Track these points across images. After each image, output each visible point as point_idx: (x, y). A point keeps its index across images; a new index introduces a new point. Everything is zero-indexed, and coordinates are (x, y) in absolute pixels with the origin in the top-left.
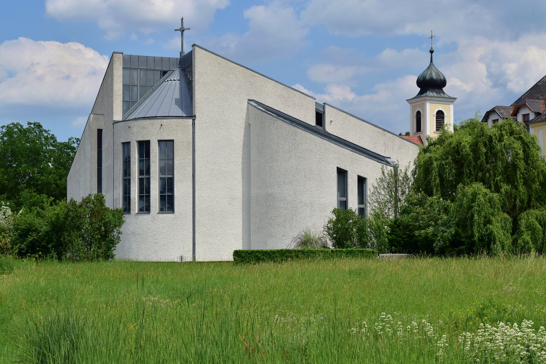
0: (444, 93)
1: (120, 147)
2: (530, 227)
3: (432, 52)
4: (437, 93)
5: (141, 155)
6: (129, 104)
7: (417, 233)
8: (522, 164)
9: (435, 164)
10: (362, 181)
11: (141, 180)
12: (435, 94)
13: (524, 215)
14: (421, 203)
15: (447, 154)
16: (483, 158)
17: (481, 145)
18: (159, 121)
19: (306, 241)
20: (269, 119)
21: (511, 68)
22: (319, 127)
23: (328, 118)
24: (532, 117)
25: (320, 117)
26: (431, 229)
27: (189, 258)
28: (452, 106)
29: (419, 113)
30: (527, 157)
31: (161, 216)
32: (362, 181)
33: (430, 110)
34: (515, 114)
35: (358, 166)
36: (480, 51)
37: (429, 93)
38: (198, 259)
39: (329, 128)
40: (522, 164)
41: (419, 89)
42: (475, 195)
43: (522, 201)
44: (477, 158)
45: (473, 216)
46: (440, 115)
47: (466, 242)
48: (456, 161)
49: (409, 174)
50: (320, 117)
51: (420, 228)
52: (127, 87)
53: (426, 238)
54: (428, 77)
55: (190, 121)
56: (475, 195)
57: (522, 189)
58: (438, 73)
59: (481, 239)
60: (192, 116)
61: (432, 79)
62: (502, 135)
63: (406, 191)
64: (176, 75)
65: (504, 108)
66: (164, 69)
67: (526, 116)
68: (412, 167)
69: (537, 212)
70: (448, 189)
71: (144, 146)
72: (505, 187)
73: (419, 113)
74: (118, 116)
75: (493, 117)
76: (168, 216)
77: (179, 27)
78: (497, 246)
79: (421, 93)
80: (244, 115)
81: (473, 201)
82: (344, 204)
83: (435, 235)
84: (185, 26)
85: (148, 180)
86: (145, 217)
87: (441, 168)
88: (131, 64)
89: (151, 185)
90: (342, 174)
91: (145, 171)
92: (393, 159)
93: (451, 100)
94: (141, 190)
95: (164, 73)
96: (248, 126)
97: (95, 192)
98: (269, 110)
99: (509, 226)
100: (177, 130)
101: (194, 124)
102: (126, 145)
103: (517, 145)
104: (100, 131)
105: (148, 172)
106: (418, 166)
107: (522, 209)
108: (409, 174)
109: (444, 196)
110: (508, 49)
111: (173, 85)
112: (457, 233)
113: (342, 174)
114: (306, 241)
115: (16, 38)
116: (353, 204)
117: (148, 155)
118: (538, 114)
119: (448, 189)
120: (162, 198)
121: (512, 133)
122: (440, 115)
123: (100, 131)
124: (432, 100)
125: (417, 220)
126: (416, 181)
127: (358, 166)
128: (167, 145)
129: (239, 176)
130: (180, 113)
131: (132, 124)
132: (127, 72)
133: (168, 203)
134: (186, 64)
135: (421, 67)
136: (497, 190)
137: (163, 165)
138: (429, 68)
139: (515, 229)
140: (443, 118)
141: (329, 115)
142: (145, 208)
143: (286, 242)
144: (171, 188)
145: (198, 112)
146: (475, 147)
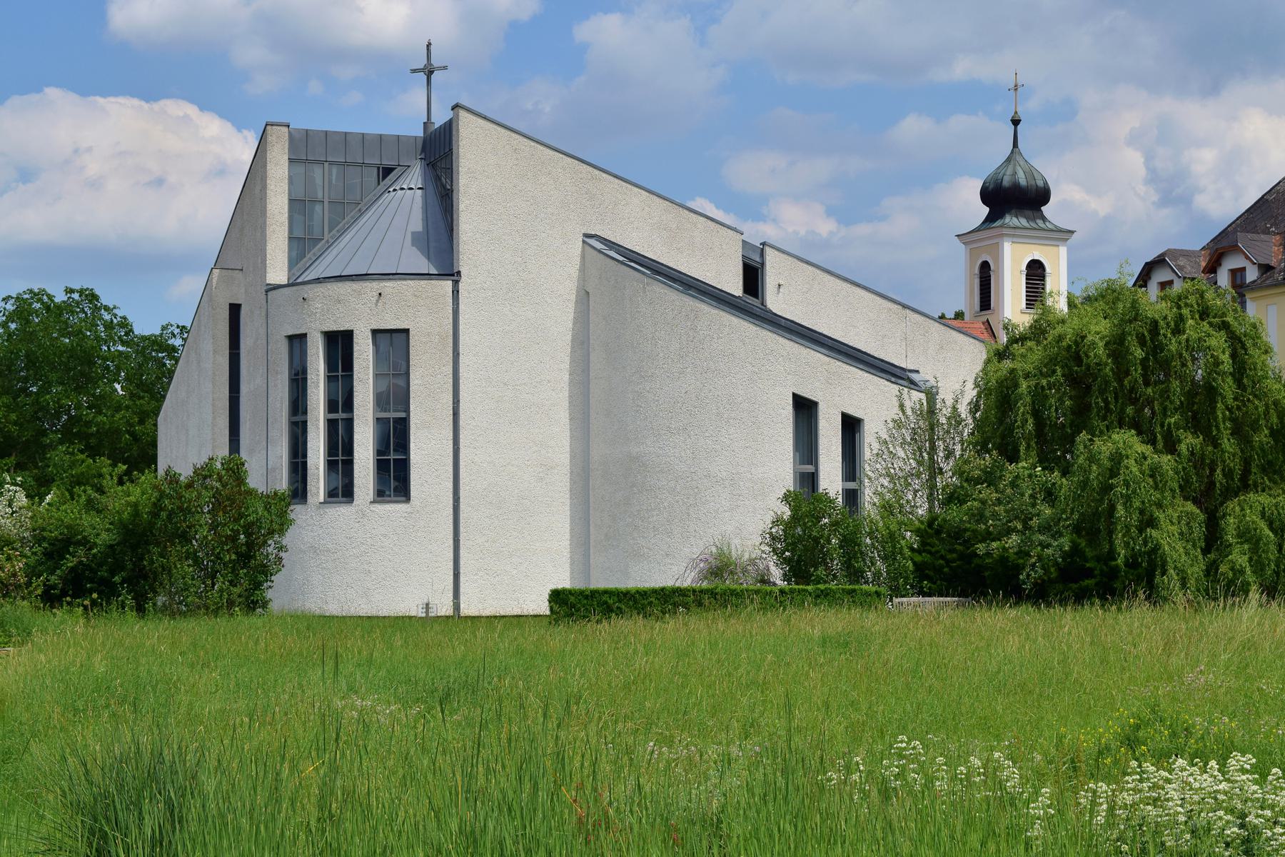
0: (1044, 219)
1: (283, 347)
2: (1246, 535)
3: (1016, 122)
4: (1028, 219)
5: (331, 365)
6: (303, 245)
7: (981, 548)
8: (1228, 387)
9: (1024, 385)
10: (851, 426)
11: (332, 425)
12: (1024, 222)
13: (1232, 505)
14: (990, 478)
15: (1052, 362)
16: (1137, 372)
17: (1132, 341)
18: (375, 286)
19: (720, 567)
20: (634, 279)
21: (1204, 160)
22: (751, 300)
23: (771, 279)
24: (1252, 275)
25: (753, 276)
26: (1014, 540)
27: (445, 608)
28: (1063, 251)
29: (985, 267)
30: (1241, 369)
31: (379, 508)
32: (851, 426)
33: (1013, 260)
34: (1212, 268)
35: (842, 392)
36: (1130, 121)
37: (1010, 220)
38: (466, 610)
39: (775, 302)
40: (1228, 387)
41: (985, 210)
42: (1117, 458)
43: (1228, 474)
44: (1122, 371)
45: (1112, 508)
46: (1036, 271)
47: (1096, 571)
48: (1072, 380)
49: (963, 410)
50: (753, 276)
51: (988, 537)
52: (298, 205)
53: (1003, 560)
54: (1007, 182)
55: (448, 285)
56: (1117, 458)
57: (1228, 444)
58: (1031, 172)
59: (1132, 564)
60: (452, 274)
61: (1016, 187)
62: (1180, 319)
63: (955, 451)
64: (414, 177)
65: (1186, 254)
66: (387, 162)
67: (1237, 274)
68: (971, 393)
69: (1264, 499)
70: (1053, 446)
71: (339, 344)
72: (1189, 441)
73: (985, 267)
74: (277, 273)
75: (1160, 276)
76: (394, 509)
77: (421, 63)
78: (1171, 579)
79: (990, 219)
80: (574, 270)
81: (1113, 473)
82: (809, 480)
83: (1024, 554)
84: (435, 62)
85: (349, 423)
86: (341, 512)
87: (1039, 395)
88: (309, 150)
89: (356, 437)
90: (805, 409)
91: (342, 402)
92: (926, 375)
93: (1062, 235)
94: (332, 448)
95: (387, 171)
96: (584, 297)
97: (224, 451)
98: (633, 259)
99: (1199, 531)
100: (416, 307)
101: (456, 292)
102: (297, 341)
103: (1218, 341)
104: (235, 310)
105: (349, 405)
106: (984, 391)
107: (1229, 493)
108: (963, 410)
109: (1046, 460)
110: (1195, 115)
111: (407, 199)
112: (1075, 549)
113: (805, 409)
114: (720, 567)
115: (39, 90)
116: (831, 480)
117: (348, 366)
118: (1266, 269)
119: (1053, 446)
120: (381, 466)
121: (1204, 314)
122: (1036, 271)
123: (235, 310)
124: (1018, 235)
125: (981, 517)
126: (979, 425)
127: (842, 392)
128: (394, 342)
129: (562, 415)
130: (424, 266)
131: (310, 291)
132: (300, 169)
133: (395, 478)
134: (438, 151)
135: (990, 157)
136: (1171, 446)
137: (383, 388)
138: (1009, 160)
139: (1213, 540)
140: (1042, 277)
141: (775, 271)
142: (342, 491)
143: (674, 570)
144: (402, 442)
145: (465, 264)
146: (1117, 346)
